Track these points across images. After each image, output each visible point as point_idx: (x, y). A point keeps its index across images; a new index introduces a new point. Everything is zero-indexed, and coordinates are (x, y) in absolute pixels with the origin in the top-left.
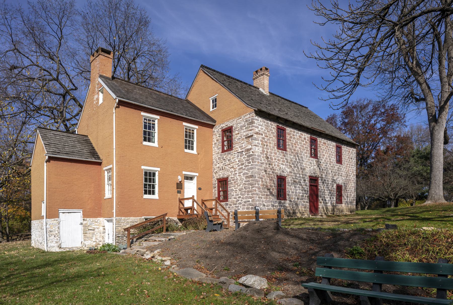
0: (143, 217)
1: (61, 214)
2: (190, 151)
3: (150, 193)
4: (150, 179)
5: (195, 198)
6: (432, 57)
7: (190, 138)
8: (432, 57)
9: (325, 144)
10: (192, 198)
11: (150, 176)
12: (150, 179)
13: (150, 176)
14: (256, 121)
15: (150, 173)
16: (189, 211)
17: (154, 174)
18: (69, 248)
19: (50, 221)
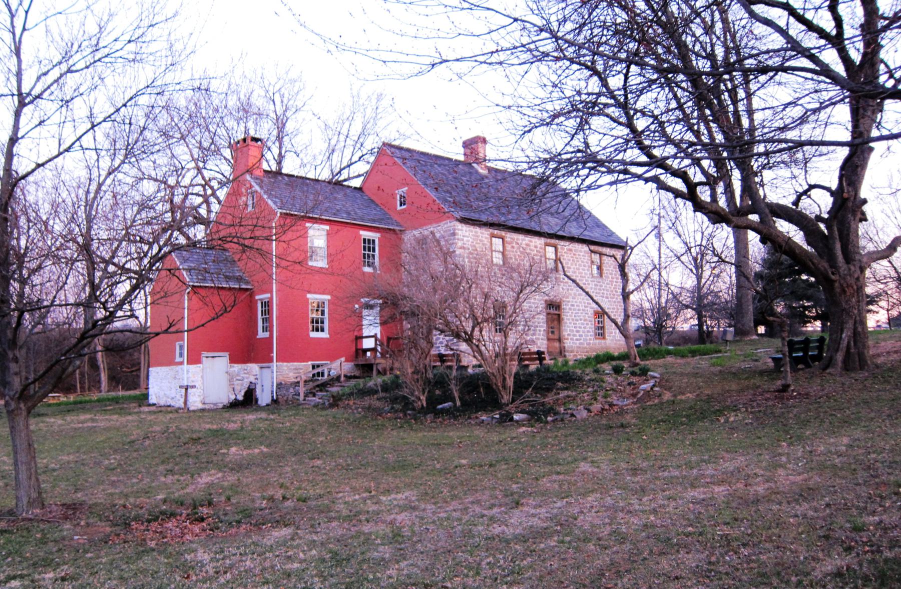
0: (310, 363)
1: (204, 359)
2: (319, 335)
3: (317, 330)
4: (369, 248)
5: (379, 336)
6: (763, 109)
7: (369, 250)
8: (763, 109)
9: (570, 250)
10: (375, 336)
11: (369, 243)
12: (369, 248)
13: (369, 243)
14: (460, 232)
15: (369, 240)
16: (369, 354)
17: (374, 241)
18: (215, 404)
19: (193, 368)
